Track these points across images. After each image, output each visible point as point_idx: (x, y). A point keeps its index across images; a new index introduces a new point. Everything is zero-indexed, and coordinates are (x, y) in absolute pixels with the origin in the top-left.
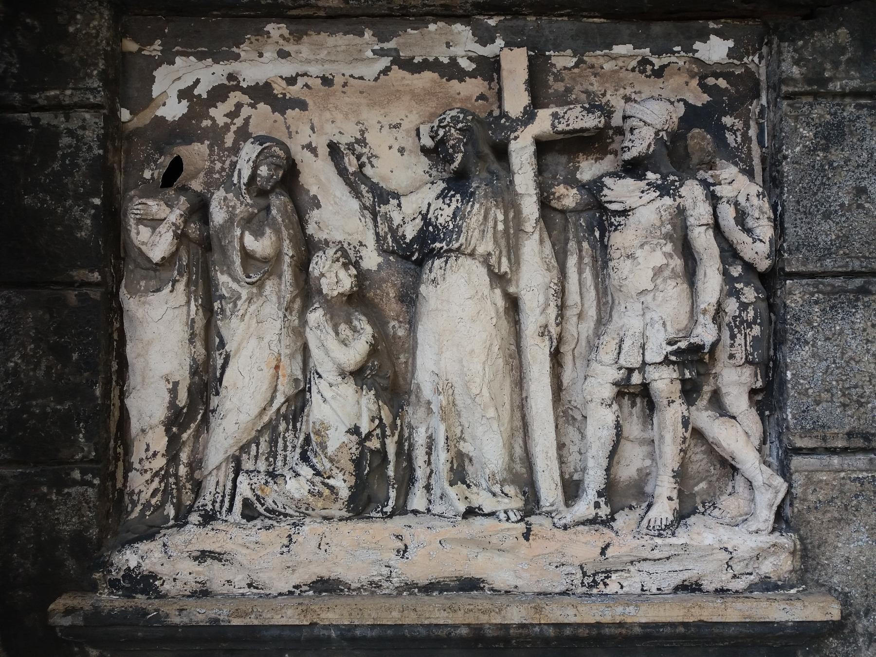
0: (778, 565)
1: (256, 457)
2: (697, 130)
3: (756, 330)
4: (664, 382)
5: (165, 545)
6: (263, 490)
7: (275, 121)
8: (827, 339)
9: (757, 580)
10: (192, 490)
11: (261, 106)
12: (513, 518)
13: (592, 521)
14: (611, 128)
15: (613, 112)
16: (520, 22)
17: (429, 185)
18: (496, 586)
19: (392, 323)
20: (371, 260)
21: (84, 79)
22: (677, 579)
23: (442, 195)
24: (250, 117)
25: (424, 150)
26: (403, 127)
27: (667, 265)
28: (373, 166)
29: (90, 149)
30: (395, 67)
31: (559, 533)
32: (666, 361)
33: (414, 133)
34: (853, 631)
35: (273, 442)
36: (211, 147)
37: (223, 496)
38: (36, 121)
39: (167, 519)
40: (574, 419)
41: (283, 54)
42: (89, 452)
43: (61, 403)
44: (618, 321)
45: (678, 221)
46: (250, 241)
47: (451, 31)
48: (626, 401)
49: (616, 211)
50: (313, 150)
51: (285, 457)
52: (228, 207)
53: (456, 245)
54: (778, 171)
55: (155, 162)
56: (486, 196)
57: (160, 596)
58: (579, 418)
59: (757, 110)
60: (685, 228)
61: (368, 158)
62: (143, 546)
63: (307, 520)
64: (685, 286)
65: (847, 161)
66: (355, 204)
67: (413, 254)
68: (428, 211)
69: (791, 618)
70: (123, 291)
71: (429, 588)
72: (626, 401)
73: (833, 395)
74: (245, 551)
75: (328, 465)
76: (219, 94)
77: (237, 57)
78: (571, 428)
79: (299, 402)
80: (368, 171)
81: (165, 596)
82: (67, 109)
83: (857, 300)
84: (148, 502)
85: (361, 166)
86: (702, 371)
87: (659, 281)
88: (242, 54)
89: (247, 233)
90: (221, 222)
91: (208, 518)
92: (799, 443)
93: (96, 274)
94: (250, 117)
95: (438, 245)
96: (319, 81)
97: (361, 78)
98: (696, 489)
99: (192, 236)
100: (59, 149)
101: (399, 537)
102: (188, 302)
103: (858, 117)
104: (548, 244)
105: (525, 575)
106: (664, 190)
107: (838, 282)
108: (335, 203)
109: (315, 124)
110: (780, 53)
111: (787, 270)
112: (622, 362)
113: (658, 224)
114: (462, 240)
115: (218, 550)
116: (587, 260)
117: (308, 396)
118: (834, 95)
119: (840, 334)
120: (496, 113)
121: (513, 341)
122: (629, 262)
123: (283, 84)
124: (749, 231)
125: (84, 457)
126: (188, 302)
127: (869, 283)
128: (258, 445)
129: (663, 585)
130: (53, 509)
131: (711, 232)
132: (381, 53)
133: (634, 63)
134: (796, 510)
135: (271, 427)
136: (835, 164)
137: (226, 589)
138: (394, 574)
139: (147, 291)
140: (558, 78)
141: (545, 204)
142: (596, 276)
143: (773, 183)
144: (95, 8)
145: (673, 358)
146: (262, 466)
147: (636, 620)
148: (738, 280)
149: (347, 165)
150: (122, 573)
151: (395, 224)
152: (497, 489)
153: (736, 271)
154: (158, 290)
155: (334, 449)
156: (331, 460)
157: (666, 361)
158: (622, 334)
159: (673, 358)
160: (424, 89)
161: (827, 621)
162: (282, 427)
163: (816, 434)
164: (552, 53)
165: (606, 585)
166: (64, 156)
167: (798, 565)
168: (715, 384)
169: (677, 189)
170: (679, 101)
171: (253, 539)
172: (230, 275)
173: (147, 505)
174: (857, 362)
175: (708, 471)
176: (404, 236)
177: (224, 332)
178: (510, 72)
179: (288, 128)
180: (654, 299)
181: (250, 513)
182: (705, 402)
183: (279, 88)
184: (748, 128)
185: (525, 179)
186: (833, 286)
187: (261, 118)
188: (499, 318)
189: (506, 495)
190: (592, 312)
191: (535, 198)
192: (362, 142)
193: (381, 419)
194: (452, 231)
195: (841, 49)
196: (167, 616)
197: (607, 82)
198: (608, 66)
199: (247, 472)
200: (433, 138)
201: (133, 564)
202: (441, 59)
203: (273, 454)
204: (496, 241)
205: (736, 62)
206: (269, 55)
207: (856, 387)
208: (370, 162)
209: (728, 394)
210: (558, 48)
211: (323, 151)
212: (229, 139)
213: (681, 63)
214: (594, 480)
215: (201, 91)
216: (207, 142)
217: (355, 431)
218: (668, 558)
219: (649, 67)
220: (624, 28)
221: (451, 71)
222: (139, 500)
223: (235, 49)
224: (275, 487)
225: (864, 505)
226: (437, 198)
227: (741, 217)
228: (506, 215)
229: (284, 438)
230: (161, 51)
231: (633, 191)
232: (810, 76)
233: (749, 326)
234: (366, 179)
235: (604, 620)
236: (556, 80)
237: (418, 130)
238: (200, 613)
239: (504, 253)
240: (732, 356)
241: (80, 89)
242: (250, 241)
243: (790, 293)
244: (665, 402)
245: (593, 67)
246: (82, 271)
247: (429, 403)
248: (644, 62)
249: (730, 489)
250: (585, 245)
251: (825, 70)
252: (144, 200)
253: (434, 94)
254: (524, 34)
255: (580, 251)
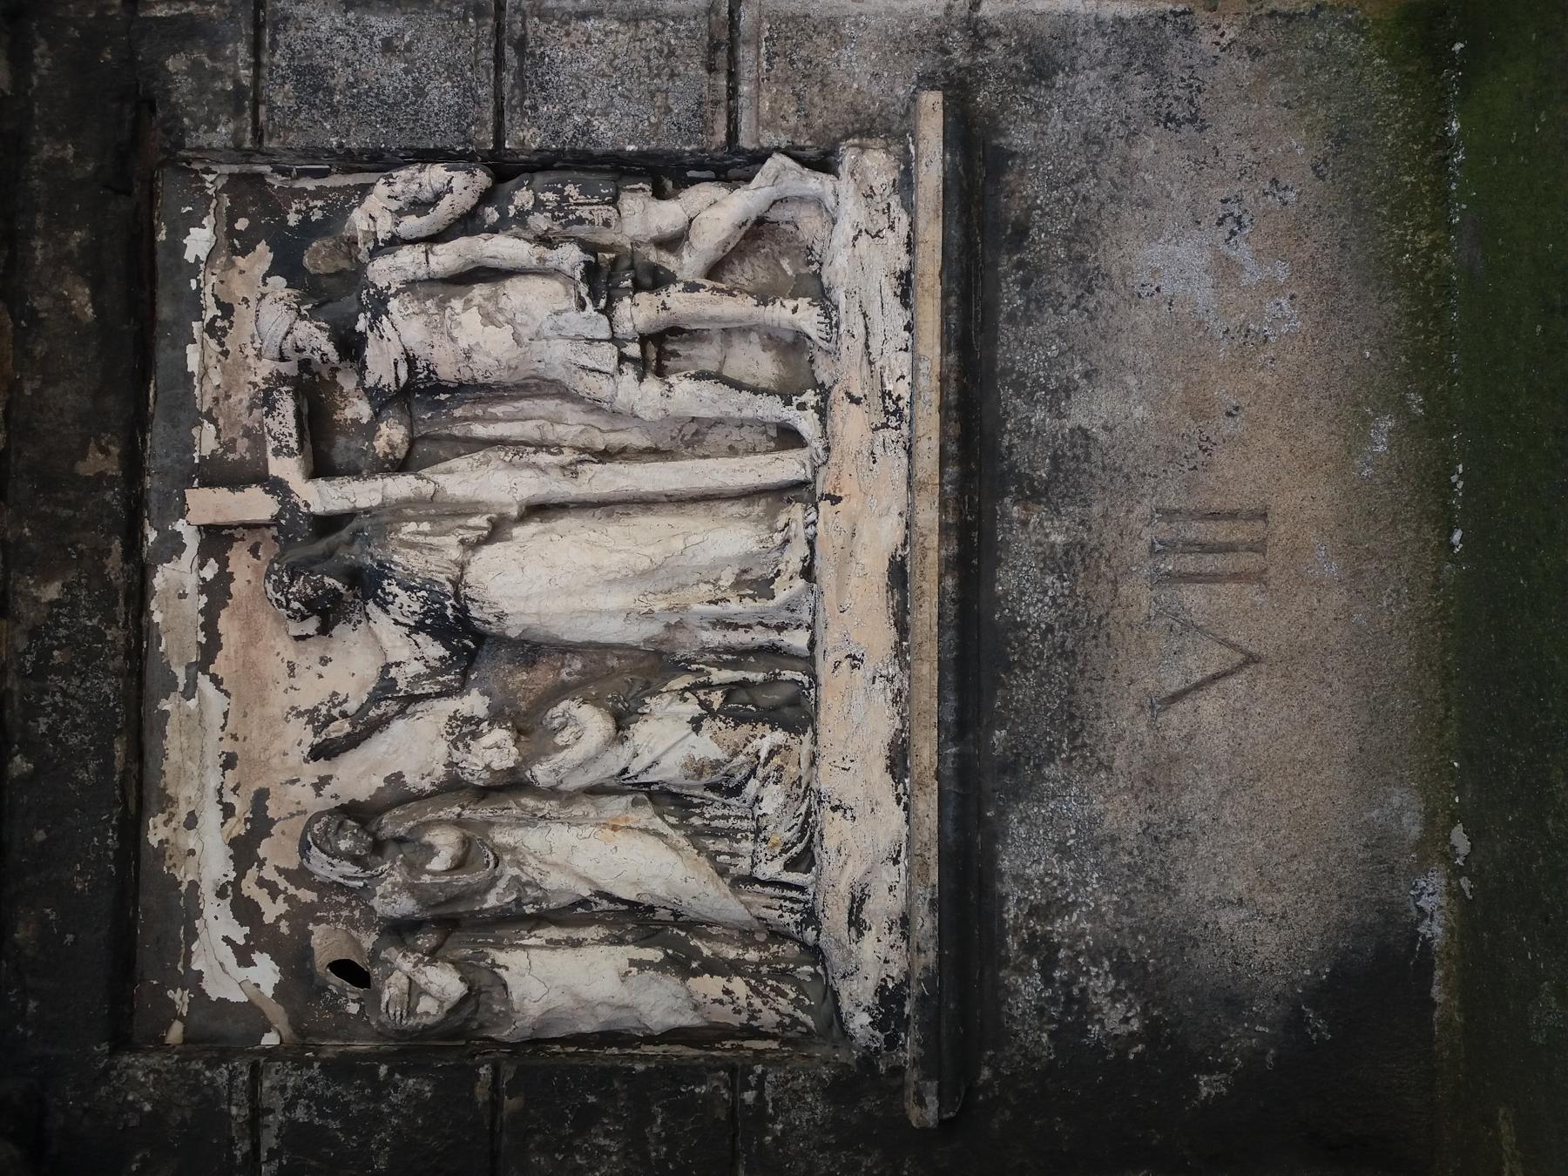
0: (877, 165)
1: (733, 855)
2: (306, 259)
3: (571, 190)
4: (637, 313)
5: (844, 977)
6: (775, 845)
7: (283, 833)
8: (584, 95)
9: (897, 198)
10: (781, 944)
11: (262, 852)
12: (812, 517)
13: (822, 412)
14: (300, 376)
15: (279, 373)
16: (153, 499)
17: (371, 624)
18: (900, 541)
19: (564, 676)
20: (474, 703)
21: (216, 1090)
22: (894, 304)
23: (383, 606)
24: (277, 868)
25: (325, 630)
26: (293, 659)
27: (479, 307)
28: (345, 701)
29: (311, 1080)
30: (212, 669)
31: (835, 457)
32: (608, 311)
33: (302, 644)
34: (969, 70)
35: (716, 834)
36: (318, 921)
37: (785, 899)
38: (273, 1154)
39: (815, 975)
40: (696, 433)
41: (192, 822)
42: (720, 1079)
43: (655, 1118)
44: (558, 373)
45: (421, 290)
46: (438, 863)
47: (163, 592)
48: (670, 363)
49: (409, 372)
50: (324, 781)
51: (737, 817)
52: (393, 892)
53: (449, 588)
54: (361, 154)
55: (336, 997)
56: (383, 546)
57: (906, 983)
58: (694, 426)
59: (280, 177)
60: (431, 280)
61: (335, 706)
62: (846, 1005)
63: (814, 786)
64: (508, 283)
65: (347, 63)
66: (398, 726)
67: (466, 647)
68: (405, 625)
69: (939, 157)
70: (504, 1034)
71: (902, 628)
72: (670, 363)
73: (659, 90)
74: (849, 868)
75: (742, 758)
76: (245, 911)
77: (194, 885)
78: (708, 438)
79: (661, 797)
80: (352, 707)
81: (908, 975)
82: (257, 1113)
83: (533, 54)
84: (792, 1001)
85: (344, 715)
86: (627, 263)
87: (501, 318)
88: (190, 877)
89: (428, 867)
90: (413, 902)
91: (811, 917)
92: (721, 136)
93: (482, 1071)
94: (277, 868)
95: (449, 612)
96: (229, 772)
97: (226, 715)
98: (790, 273)
99: (434, 942)
100: (311, 1122)
101: (837, 665)
102: (524, 947)
103: (288, 46)
104: (455, 463)
105: (884, 504)
106: (379, 306)
107: (508, 78)
108: (395, 752)
109: (288, 777)
110: (199, 149)
111: (491, 147)
112: (610, 369)
113: (424, 318)
114: (442, 578)
115: (848, 902)
116: (479, 412)
117: (656, 787)
118: (257, 77)
119: (578, 79)
120: (274, 531)
121: (590, 513)
122: (475, 357)
123: (232, 821)
124: (438, 196)
125: (726, 1086)
126: (524, 947)
127: (510, 39)
128: (719, 853)
129: (901, 322)
130: (795, 1128)
131: (438, 248)
132: (190, 691)
133: (213, 343)
134: (809, 143)
135: (695, 836)
136: (351, 79)
137: (901, 894)
138: (884, 672)
139: (507, 1001)
140: (230, 446)
141: (401, 466)
142: (501, 399)
143: (381, 162)
144: (120, 1075)
145: (603, 303)
146: (747, 846)
147: (937, 360)
148: (503, 213)
149: (341, 734)
150: (877, 1033)
151: (424, 670)
152: (778, 538)
153: (491, 214)
154: (505, 986)
155: (719, 751)
156: (735, 754)
157: (608, 311)
158: (574, 368)
159: (603, 303)
160: (242, 629)
161: (945, 110)
162: (696, 821)
163: (709, 114)
164: (196, 455)
165: (899, 398)
166: (322, 1115)
167: (879, 142)
168: (647, 244)
169: (379, 292)
170: (265, 284)
171: (833, 855)
172: (487, 891)
173: (797, 1003)
174: (616, 57)
175: (767, 256)
176: (441, 659)
177: (565, 900)
178: (218, 512)
179: (292, 815)
180: (525, 325)
181: (803, 860)
182: (672, 259)
183: (238, 828)
184: (305, 190)
185: (362, 494)
186: (513, 86)
187: (277, 852)
188: (553, 530)
189: (787, 525)
190: (551, 405)
191: (388, 480)
192: (312, 715)
193: (686, 689)
194: (431, 591)
195: (195, 68)
196: (926, 968)
197: (237, 381)
198: (216, 378)
199: (753, 865)
200: (304, 618)
201: (865, 1019)
202: (202, 606)
203: (730, 834)
204: (445, 534)
205: (213, 205)
206: (190, 840)
207: (648, 59)
208: (340, 704)
209: (659, 229)
210: (190, 448)
211: (321, 767)
212: (307, 896)
213: (214, 279)
214: (771, 409)
215: (239, 934)
216: (311, 927)
217: (696, 724)
218: (865, 315)
219: (219, 323)
220: (163, 356)
221: (217, 592)
222: (789, 1016)
223: (183, 888)
224: (770, 828)
225: (804, 53)
226: (387, 612)
227: (419, 206)
228: (408, 519)
229: (713, 818)
230: (183, 989)
231: (381, 349)
232: (230, 109)
233: (565, 199)
234: (363, 709)
235: (937, 403)
236: (234, 450)
237: (297, 638)
238: (925, 923)
239: (461, 522)
240: (606, 223)
241: (230, 1093)
242: (438, 863)
243: (522, 143)
244: (664, 314)
245: (216, 400)
246: (478, 1090)
247: (668, 626)
248: (211, 329)
249: (790, 228)
250: (458, 413)
251: (223, 90)
252: (383, 1005)
253: (249, 616)
254: (170, 493)
255: (466, 419)
